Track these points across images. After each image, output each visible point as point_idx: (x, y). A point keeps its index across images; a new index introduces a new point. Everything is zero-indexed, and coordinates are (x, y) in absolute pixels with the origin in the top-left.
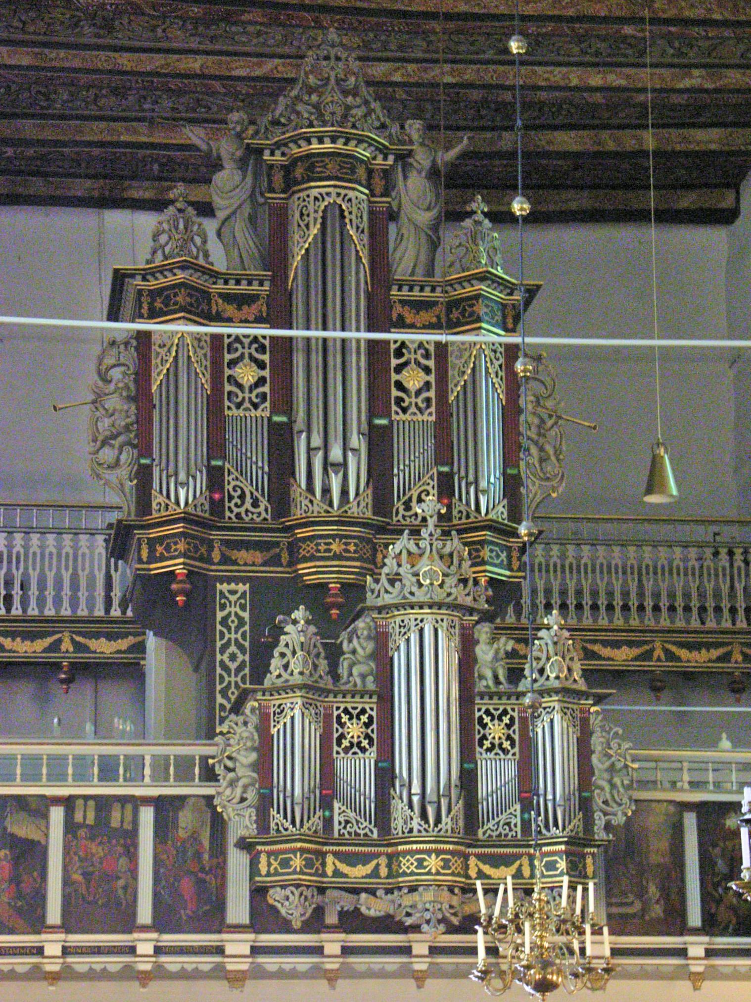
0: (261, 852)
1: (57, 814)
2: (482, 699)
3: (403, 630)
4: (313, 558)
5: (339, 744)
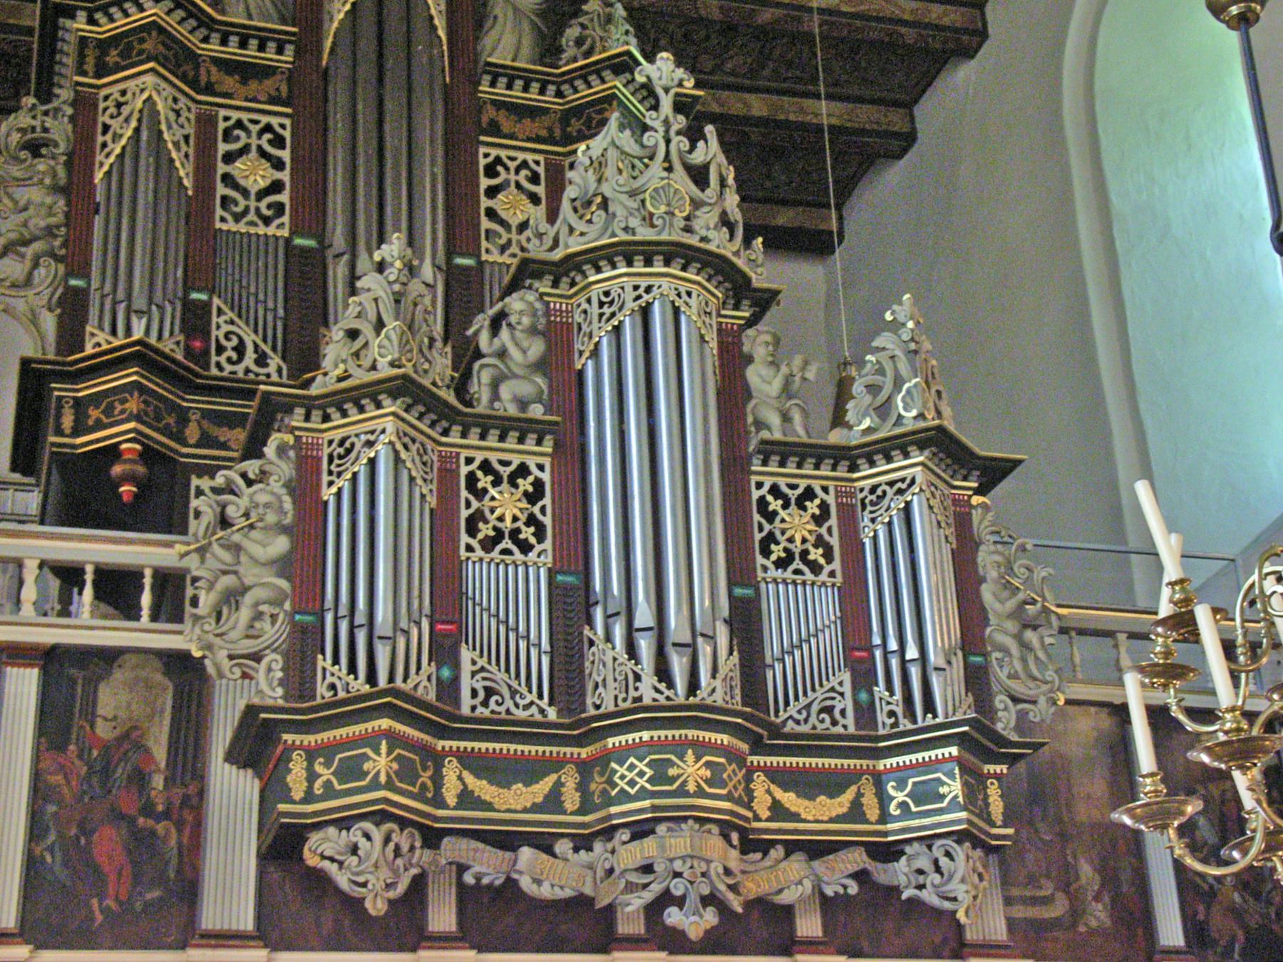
0: (294, 747)
2: (765, 463)
5: (472, 531)
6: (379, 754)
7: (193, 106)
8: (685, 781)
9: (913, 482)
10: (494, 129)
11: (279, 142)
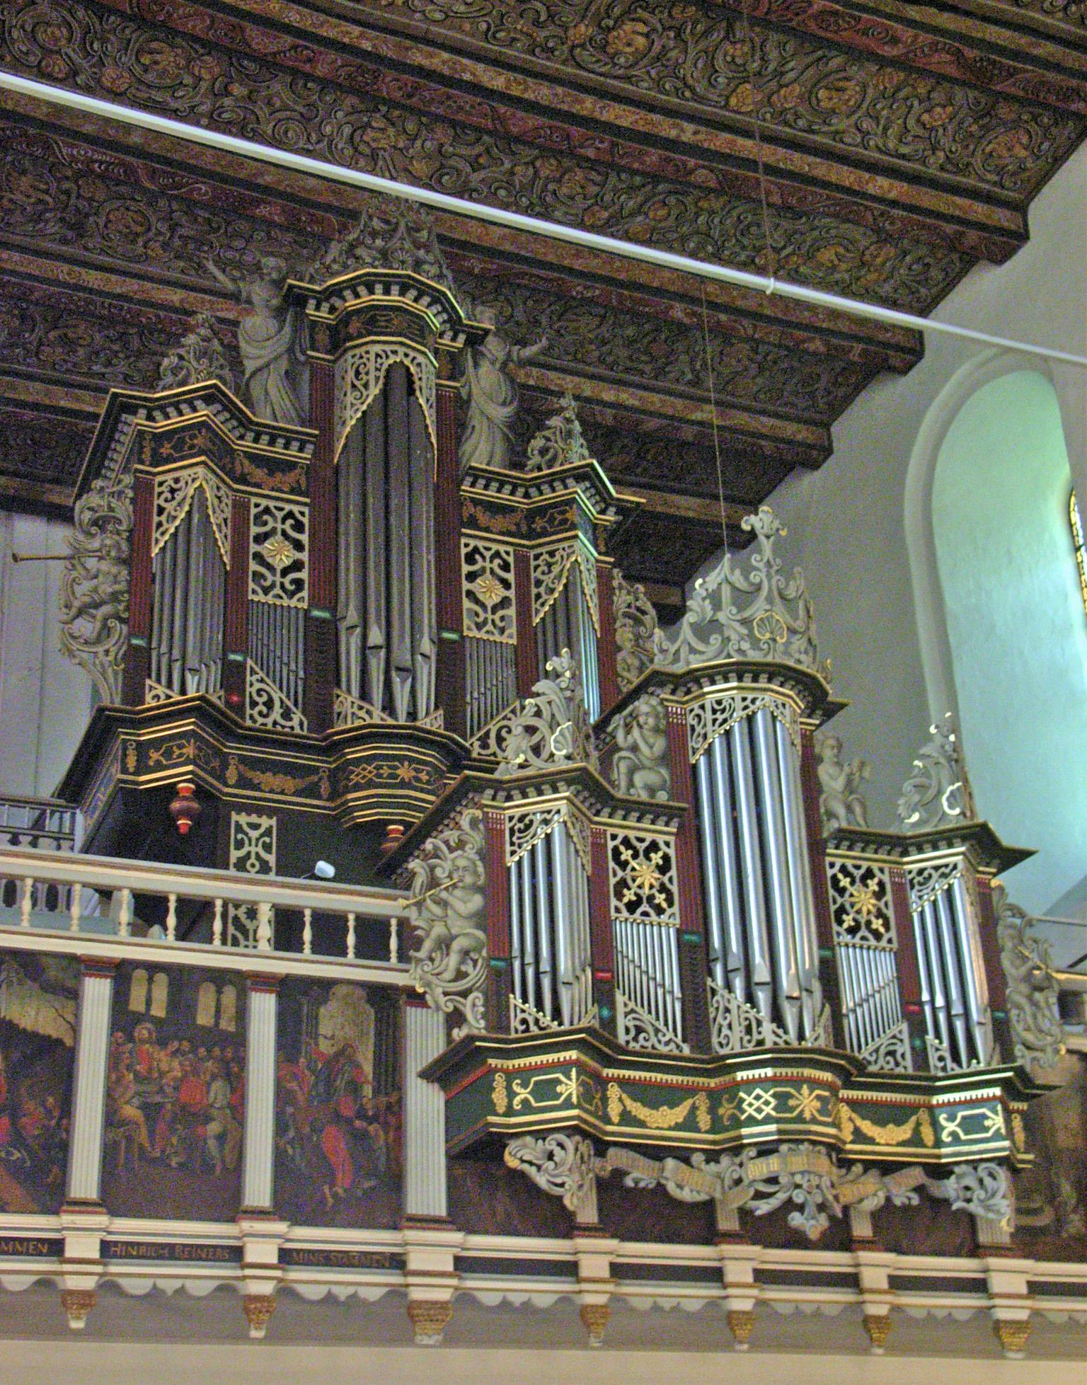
0: (496, 1070)
1: (97, 992)
3: (720, 717)
4: (370, 784)
5: (619, 896)
6: (570, 1079)
7: (230, 494)
8: (802, 1111)
9: (955, 867)
10: (473, 523)
11: (299, 527)
